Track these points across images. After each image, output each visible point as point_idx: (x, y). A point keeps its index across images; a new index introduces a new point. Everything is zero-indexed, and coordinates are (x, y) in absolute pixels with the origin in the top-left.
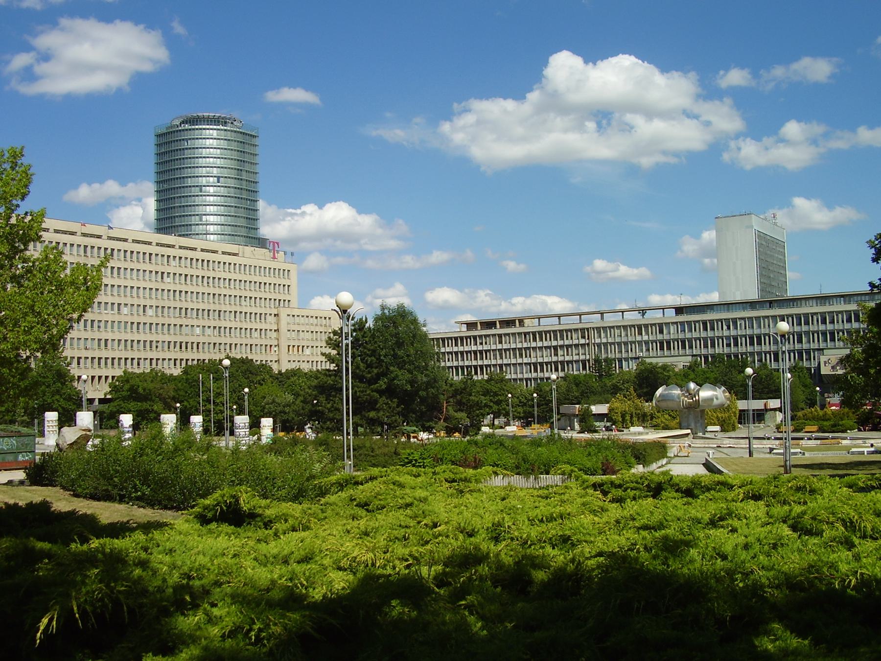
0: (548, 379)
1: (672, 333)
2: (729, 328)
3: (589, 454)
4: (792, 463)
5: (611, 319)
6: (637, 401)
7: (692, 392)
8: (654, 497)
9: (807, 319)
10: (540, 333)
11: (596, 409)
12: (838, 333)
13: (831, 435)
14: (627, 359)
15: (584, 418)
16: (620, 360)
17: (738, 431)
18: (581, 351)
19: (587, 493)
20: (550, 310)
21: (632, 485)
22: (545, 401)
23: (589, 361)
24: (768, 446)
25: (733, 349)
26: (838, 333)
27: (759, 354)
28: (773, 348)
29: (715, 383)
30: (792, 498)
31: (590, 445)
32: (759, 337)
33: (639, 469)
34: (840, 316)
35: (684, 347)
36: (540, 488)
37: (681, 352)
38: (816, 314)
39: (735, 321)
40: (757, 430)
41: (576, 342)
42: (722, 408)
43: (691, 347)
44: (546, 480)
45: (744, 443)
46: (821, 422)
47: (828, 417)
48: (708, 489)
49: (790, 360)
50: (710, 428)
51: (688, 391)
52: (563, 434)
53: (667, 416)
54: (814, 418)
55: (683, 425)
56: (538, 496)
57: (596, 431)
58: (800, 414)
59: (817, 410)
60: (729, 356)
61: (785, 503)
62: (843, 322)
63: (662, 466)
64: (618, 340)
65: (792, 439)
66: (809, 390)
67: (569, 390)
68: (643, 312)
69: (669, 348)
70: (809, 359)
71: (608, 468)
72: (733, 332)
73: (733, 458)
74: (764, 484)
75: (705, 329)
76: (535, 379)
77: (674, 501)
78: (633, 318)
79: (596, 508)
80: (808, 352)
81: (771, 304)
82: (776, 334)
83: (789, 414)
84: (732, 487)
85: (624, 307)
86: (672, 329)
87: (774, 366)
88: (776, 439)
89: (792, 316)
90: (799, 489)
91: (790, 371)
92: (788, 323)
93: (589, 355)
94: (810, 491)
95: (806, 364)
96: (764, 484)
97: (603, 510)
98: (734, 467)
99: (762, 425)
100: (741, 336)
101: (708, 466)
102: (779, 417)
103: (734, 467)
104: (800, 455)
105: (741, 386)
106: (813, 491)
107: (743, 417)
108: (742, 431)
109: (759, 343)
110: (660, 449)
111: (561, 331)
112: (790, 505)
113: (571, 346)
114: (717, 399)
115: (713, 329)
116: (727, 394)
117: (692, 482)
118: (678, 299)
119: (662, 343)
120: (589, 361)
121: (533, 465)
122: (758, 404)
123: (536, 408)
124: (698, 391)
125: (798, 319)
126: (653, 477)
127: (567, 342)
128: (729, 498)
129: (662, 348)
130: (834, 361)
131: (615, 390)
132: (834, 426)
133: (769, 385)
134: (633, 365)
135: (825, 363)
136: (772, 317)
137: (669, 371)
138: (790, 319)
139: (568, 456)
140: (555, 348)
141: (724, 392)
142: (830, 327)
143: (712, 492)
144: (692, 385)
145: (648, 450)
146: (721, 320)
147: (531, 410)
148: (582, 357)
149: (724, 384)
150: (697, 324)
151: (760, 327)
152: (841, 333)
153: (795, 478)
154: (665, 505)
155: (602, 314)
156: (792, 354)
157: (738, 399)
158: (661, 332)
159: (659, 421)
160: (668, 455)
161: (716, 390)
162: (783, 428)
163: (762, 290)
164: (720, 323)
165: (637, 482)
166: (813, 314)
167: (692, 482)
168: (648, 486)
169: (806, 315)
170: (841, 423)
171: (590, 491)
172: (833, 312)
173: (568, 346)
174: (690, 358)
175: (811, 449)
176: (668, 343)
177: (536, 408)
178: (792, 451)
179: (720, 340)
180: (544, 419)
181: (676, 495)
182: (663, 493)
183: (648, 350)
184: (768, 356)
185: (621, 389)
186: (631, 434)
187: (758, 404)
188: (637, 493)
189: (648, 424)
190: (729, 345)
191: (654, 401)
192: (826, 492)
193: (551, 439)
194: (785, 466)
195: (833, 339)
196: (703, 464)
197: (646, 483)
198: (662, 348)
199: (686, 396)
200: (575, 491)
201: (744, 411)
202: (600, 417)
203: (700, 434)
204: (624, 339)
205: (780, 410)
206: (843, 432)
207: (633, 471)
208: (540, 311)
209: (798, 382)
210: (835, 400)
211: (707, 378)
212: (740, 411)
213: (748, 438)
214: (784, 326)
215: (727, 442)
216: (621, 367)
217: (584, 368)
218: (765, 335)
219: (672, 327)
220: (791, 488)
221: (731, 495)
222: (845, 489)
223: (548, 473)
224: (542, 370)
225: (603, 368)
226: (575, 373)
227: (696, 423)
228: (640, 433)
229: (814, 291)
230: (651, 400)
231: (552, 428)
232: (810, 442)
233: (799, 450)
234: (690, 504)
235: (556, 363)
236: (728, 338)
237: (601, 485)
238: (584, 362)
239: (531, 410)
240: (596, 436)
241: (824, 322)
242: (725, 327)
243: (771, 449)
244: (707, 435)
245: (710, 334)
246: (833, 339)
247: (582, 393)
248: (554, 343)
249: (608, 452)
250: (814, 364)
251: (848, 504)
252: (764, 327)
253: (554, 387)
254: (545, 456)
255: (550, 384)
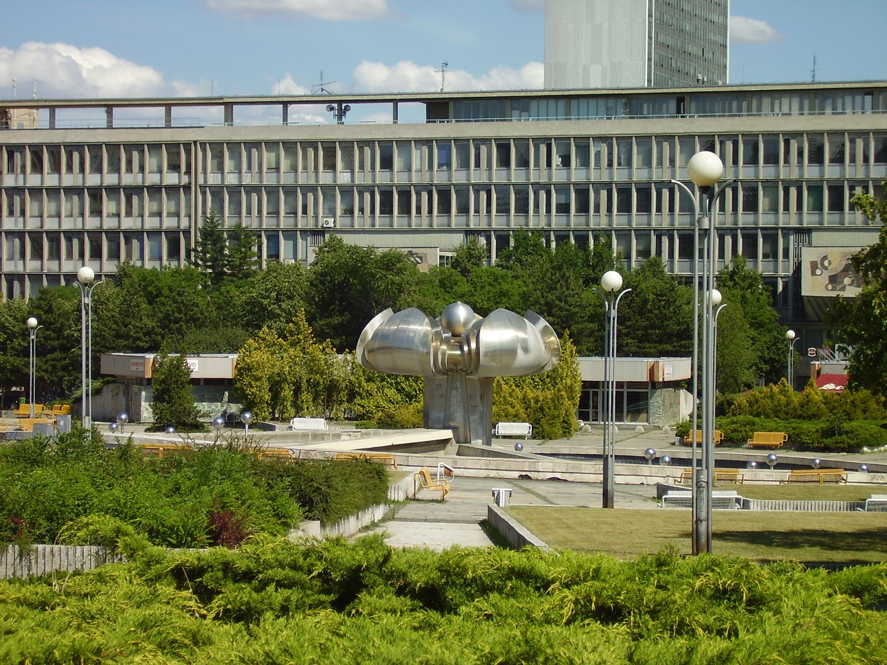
0: (72, 277)
1: (416, 169)
2: (566, 162)
3: (177, 489)
4: (715, 528)
5: (253, 122)
6: (315, 349)
7: (461, 330)
8: (339, 606)
9: (772, 147)
10: (54, 149)
11: (204, 366)
12: (852, 188)
13: (818, 457)
14: (291, 234)
15: (166, 391)
16: (273, 237)
17: (576, 437)
18: (167, 205)
19: (155, 595)
20: (96, 88)
21: (280, 574)
22: (58, 341)
23: (187, 233)
24: (653, 481)
25: (575, 220)
26: (852, 188)
27: (643, 234)
28: (680, 221)
29: (523, 307)
30: (700, 618)
31: (179, 466)
32: (644, 192)
33: (311, 531)
34: (860, 143)
35: (445, 208)
36: (31, 580)
37: (438, 220)
38: (797, 135)
39: (583, 144)
40: (627, 435)
41: (152, 179)
42: (537, 374)
43: (464, 209)
44: (50, 557)
45: (592, 471)
46: (795, 423)
47: (813, 410)
48: (485, 590)
49: (722, 255)
50: (504, 428)
51: (450, 326)
52: (109, 434)
53: (391, 392)
54: (776, 413)
55: (435, 415)
56: (19, 602)
57: (197, 427)
58: (741, 398)
59: (785, 391)
60: (562, 237)
61: (681, 629)
62: (866, 159)
63: (374, 525)
64: (269, 179)
65: (720, 463)
66: (767, 338)
67: (128, 311)
68: (340, 107)
69: (405, 209)
70: (771, 254)
71: (224, 527)
72: (577, 175)
73: (561, 510)
74: (631, 579)
75: (505, 162)
76: (36, 278)
77: (388, 620)
78: (313, 120)
79: (178, 636)
80: (771, 236)
81: (681, 103)
82: (689, 184)
83: (711, 394)
84: (546, 584)
85: (288, 87)
86: (418, 157)
87: (680, 268)
88: (676, 461)
89: (733, 137)
90: (721, 594)
91: (722, 282)
92: (723, 157)
93: (187, 217)
94: (750, 602)
95: (763, 267)
96: (631, 579)
97: (198, 640)
98: (562, 533)
99: (640, 425)
100: (598, 186)
101: (495, 528)
102: (686, 404)
103: (562, 533)
104: (736, 508)
105: (592, 318)
106: (756, 603)
107: (590, 400)
108: (587, 438)
109: (644, 207)
110: (369, 479)
111: (113, 148)
112: (692, 633)
113: (138, 190)
114: (526, 350)
115: (524, 162)
116: (553, 339)
117: (440, 569)
118: (438, 76)
119: (387, 196)
120: (187, 233)
121: (15, 516)
122: (632, 369)
123: (33, 359)
124: (478, 327)
125: (751, 147)
126: (338, 551)
127: (128, 179)
128: (538, 614)
129: (387, 209)
130: (837, 261)
131: (255, 317)
132: (828, 433)
133: (663, 318)
134: (308, 252)
135: (814, 266)
136: (682, 137)
137: (400, 271)
138: (729, 146)
139: (117, 492)
140: (96, 193)
141: (544, 332)
142: (831, 171)
143: (494, 597)
144: (462, 312)
145: (338, 482)
146: (547, 141)
147: (18, 362)
148: (169, 223)
149: (547, 310)
150: (484, 149)
151: (648, 163)
152: (859, 191)
153: (713, 565)
154: (360, 628)
155: (229, 106)
156: (728, 240)
157: (580, 353)
158: (387, 163)
159: (370, 404)
160: (392, 495)
161: (523, 328)
162: (695, 436)
163: (660, 65)
164: (543, 148)
165: (294, 567)
166: (789, 136)
167: (440, 569)
168: (324, 576)
169: (771, 138)
170: (846, 426)
171: (167, 589)
172: (841, 133)
173: (132, 191)
174: (458, 239)
175: (765, 493)
176: (405, 195)
177: (33, 359)
178: (716, 494)
179: (543, 195)
180: (53, 390)
181: (396, 602)
182: (363, 596)
183: (349, 212)
184: (665, 241)
185: (273, 316)
186: (295, 437)
187: (632, 369)
188: (294, 595)
189: (340, 410)
190: (564, 208)
191: (359, 351)
192: (788, 605)
193: (73, 446)
194: (694, 535)
195: (837, 205)
196: (483, 524)
197: (319, 568)
198: (387, 209)
199: (446, 341)
200: (124, 587)
201: (594, 384)
202: (213, 387)
203: (478, 443)
204: (286, 179)
205: (688, 385)
206: (853, 449)
207: (294, 536)
208: (61, 86)
209: (739, 314)
210: (833, 365)
211: (503, 294)
212: (587, 385)
213: (604, 458)
214: (709, 163)
215: (547, 467)
216: (274, 255)
217: (174, 252)
218: (660, 185)
219: (415, 154)
220: (701, 591)
221: (541, 606)
222: (839, 597)
223: (53, 541)
224: (55, 254)
225: (223, 253)
226: (148, 265)
227: (467, 412)
228: (317, 436)
229: (796, 75)
230: (352, 347)
231: (76, 413)
232: (763, 474)
233: (734, 495)
234: (432, 627)
235: (95, 235)
236: (563, 189)
237: (197, 572)
238: (173, 237)
239: (18, 362)
240: (199, 439)
241: (817, 157)
242: (556, 160)
243: (662, 490)
244: (496, 446)
245: (516, 175)
246: (837, 205)
247: (166, 322)
248: (93, 180)
249: (226, 485)
250: (784, 269)
251: (846, 640)
252: (660, 163)
253: (87, 300)
254: (50, 492)
255: (77, 293)
